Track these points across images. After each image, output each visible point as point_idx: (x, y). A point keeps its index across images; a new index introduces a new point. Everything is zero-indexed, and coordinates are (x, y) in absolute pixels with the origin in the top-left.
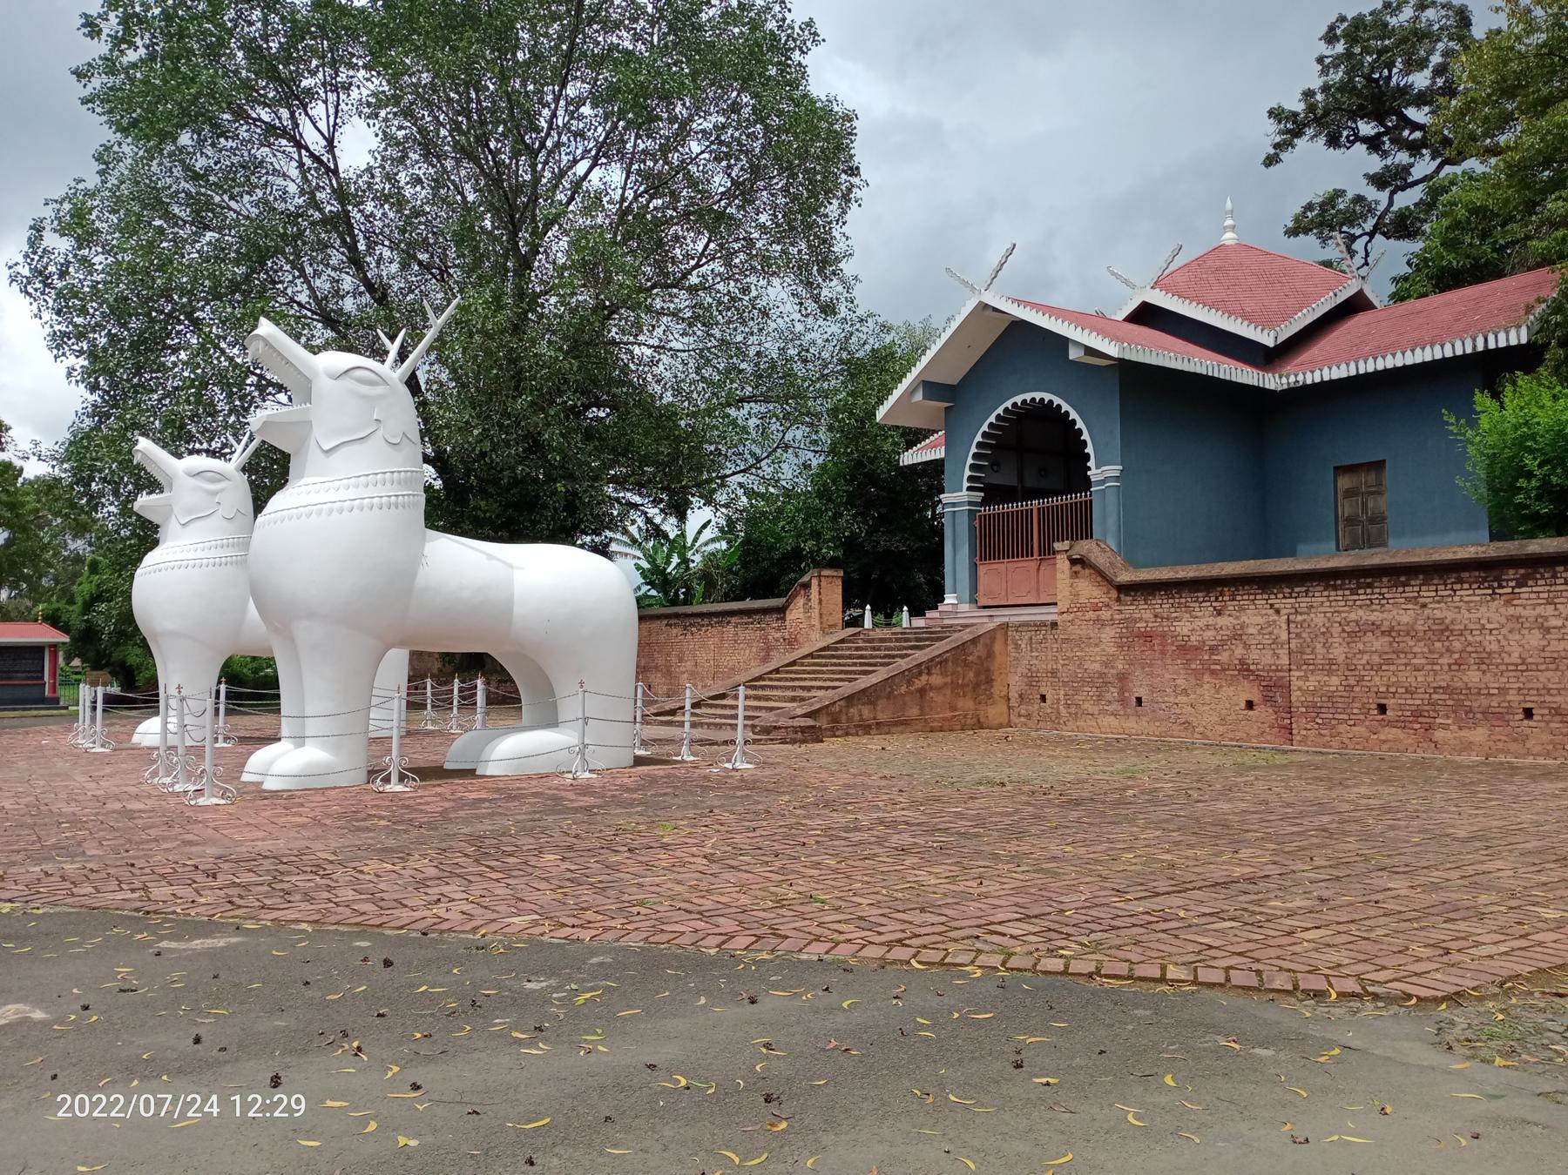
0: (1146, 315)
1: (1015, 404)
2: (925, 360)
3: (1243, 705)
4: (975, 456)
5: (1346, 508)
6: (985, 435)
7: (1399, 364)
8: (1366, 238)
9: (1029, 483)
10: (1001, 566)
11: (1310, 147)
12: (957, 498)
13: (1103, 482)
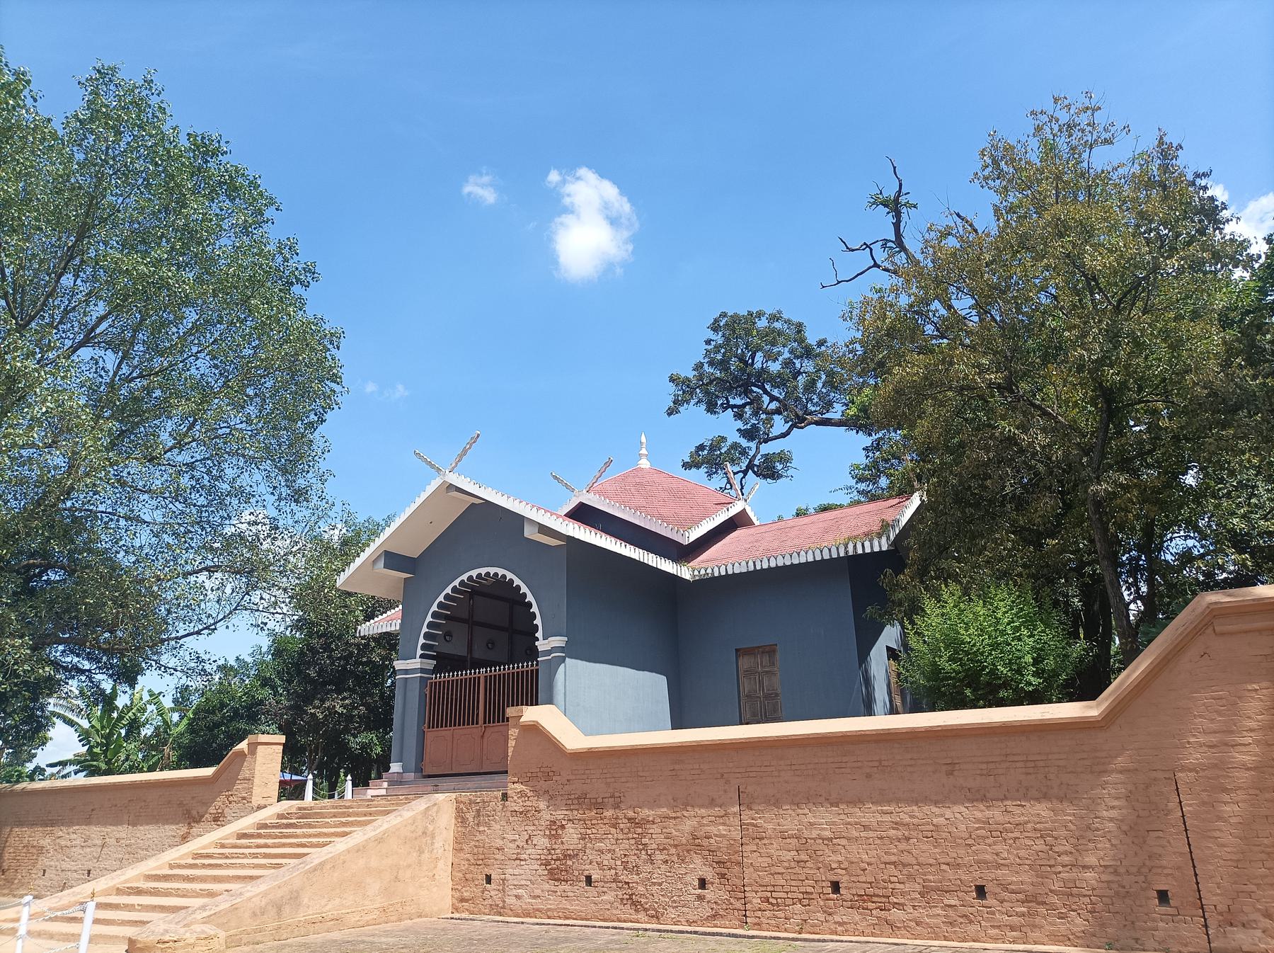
0: (582, 514)
1: (470, 578)
2: (388, 532)
3: (696, 883)
4: (430, 625)
5: (747, 686)
6: (440, 605)
7: (788, 563)
8: (741, 475)
9: (478, 654)
10: (446, 732)
11: (694, 412)
12: (410, 665)
13: (548, 653)
